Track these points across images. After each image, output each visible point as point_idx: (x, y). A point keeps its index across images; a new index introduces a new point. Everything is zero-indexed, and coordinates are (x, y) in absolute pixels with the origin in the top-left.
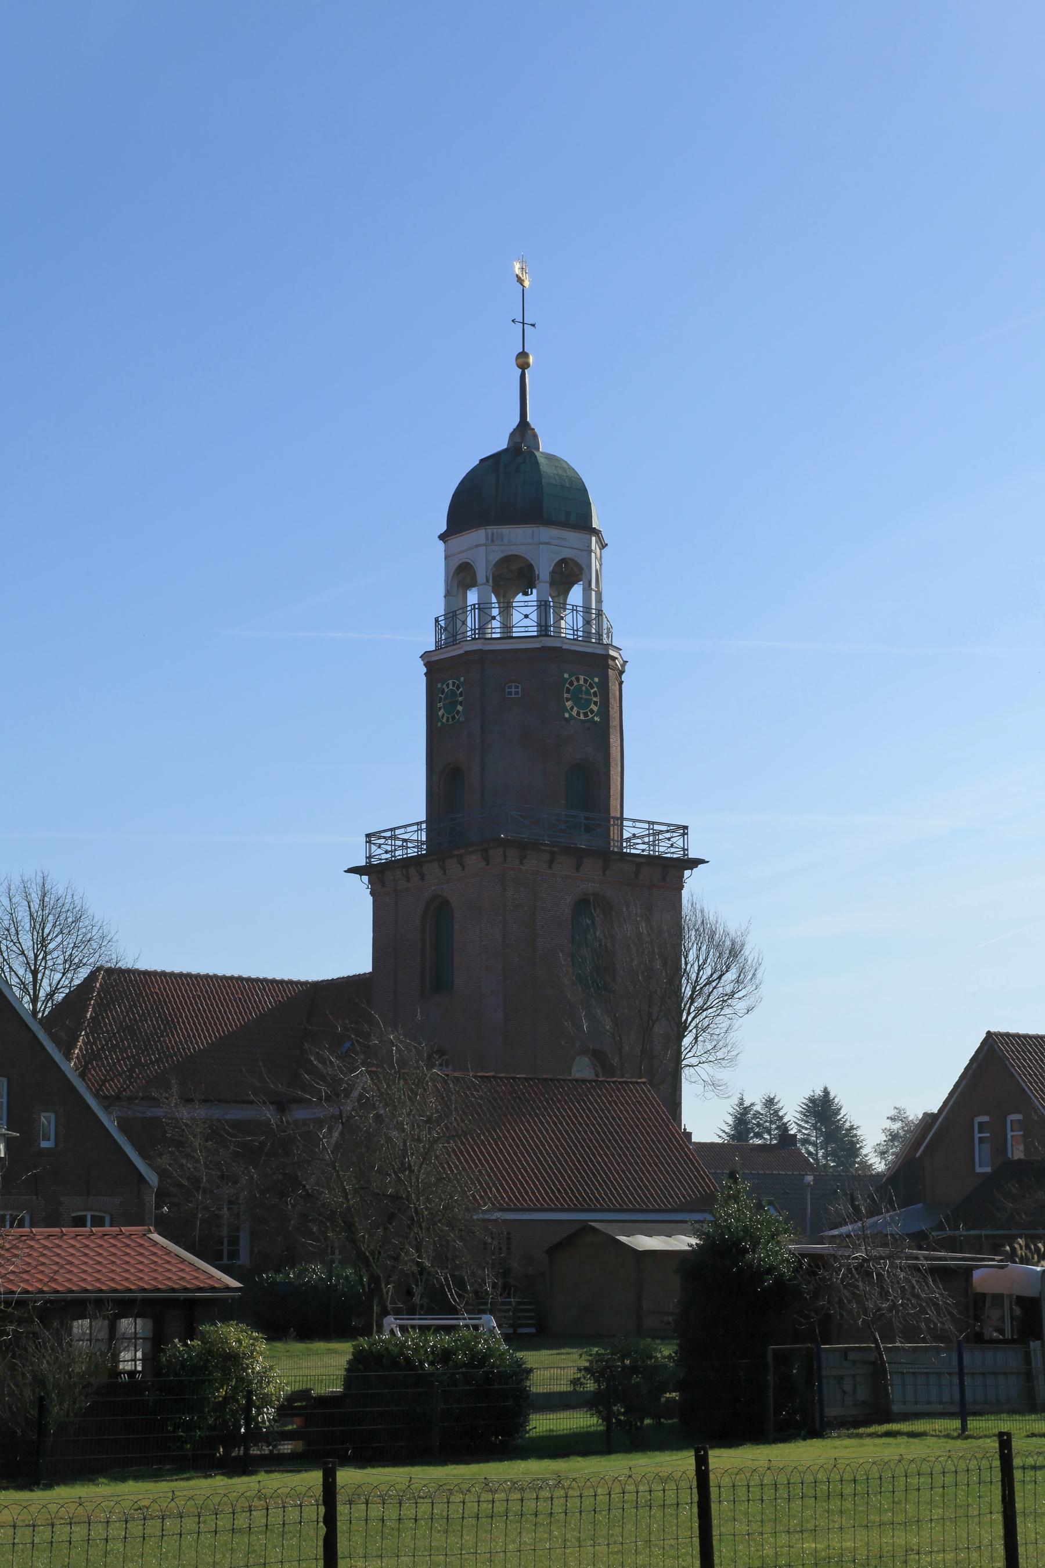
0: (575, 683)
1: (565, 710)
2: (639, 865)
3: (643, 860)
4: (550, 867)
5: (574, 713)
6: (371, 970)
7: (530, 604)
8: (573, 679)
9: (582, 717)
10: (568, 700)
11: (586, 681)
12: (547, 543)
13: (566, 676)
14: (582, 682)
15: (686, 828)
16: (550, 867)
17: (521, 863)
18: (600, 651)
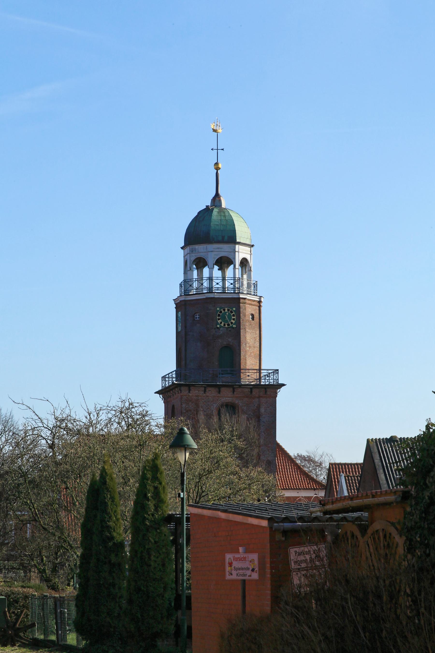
0: (223, 312)
1: (217, 324)
2: (251, 389)
3: (251, 387)
4: (205, 393)
5: (222, 325)
6: (361, 460)
7: (219, 278)
8: (222, 310)
9: (226, 326)
10: (219, 319)
11: (228, 310)
12: (212, 251)
13: (218, 309)
14: (226, 311)
15: (278, 370)
16: (205, 393)
17: (189, 392)
18: (235, 296)
